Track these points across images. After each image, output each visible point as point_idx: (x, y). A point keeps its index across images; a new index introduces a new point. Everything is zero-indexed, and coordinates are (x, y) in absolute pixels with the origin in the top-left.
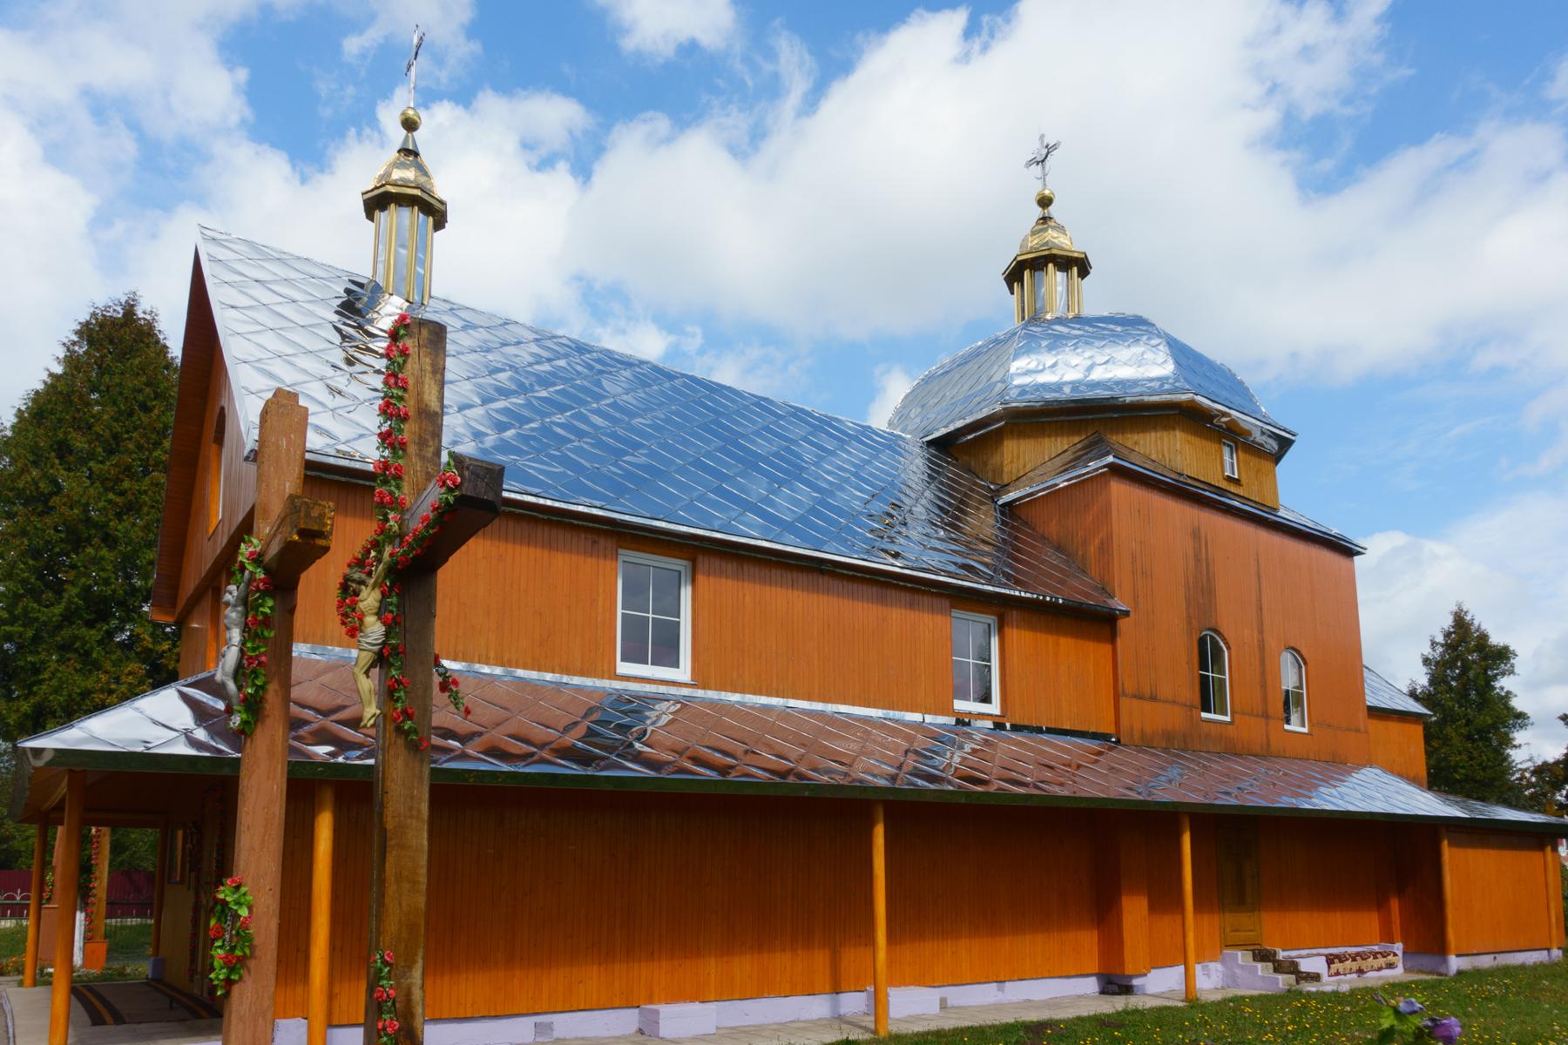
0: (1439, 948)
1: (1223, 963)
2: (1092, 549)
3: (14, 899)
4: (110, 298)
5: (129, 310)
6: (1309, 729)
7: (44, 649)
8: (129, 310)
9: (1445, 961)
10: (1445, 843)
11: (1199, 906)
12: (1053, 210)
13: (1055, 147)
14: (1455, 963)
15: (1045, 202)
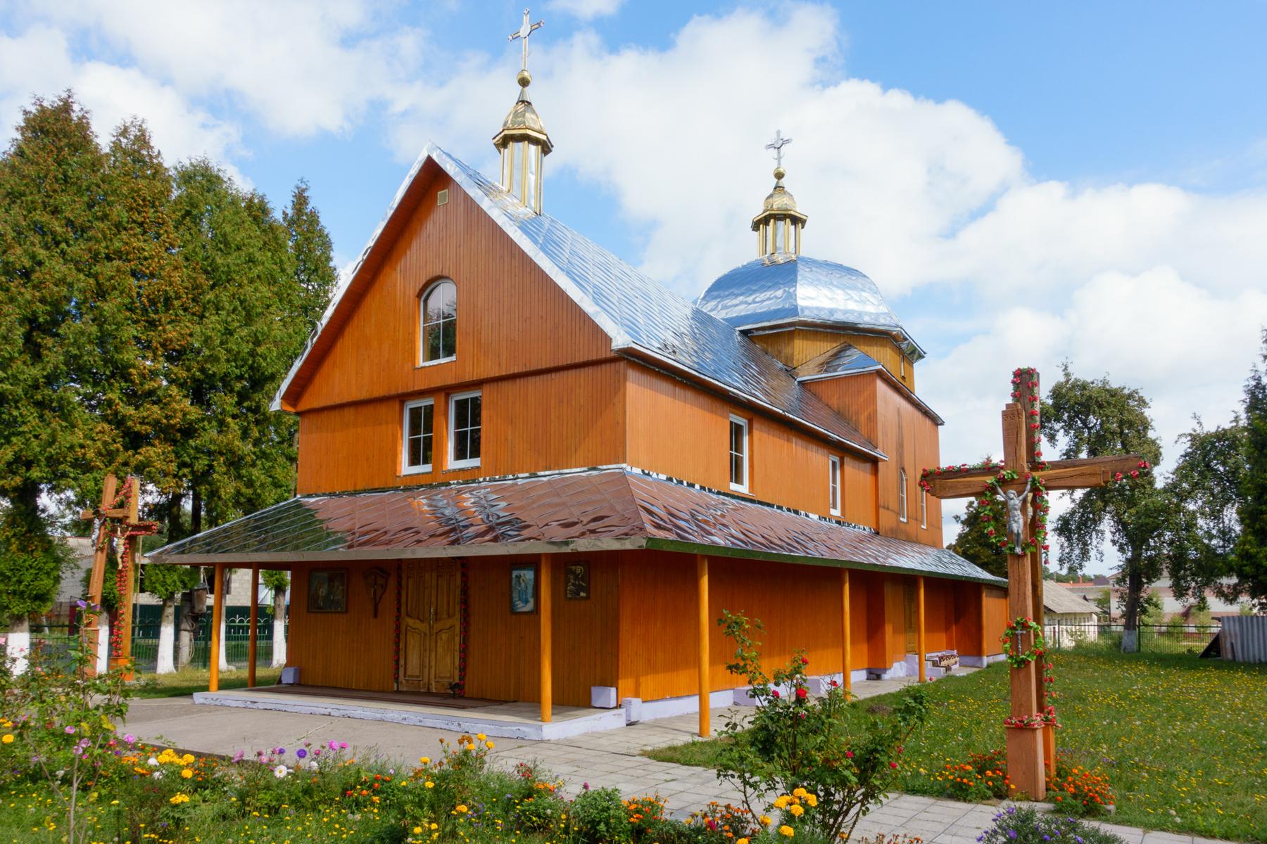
0: (979, 653)
1: (906, 662)
2: (863, 418)
3: (235, 622)
4: (143, 121)
5: (66, 107)
6: (927, 527)
7: (23, 405)
8: (66, 107)
9: (981, 660)
10: (984, 595)
11: (928, 630)
12: (783, 182)
13: (788, 141)
14: (986, 660)
15: (779, 176)
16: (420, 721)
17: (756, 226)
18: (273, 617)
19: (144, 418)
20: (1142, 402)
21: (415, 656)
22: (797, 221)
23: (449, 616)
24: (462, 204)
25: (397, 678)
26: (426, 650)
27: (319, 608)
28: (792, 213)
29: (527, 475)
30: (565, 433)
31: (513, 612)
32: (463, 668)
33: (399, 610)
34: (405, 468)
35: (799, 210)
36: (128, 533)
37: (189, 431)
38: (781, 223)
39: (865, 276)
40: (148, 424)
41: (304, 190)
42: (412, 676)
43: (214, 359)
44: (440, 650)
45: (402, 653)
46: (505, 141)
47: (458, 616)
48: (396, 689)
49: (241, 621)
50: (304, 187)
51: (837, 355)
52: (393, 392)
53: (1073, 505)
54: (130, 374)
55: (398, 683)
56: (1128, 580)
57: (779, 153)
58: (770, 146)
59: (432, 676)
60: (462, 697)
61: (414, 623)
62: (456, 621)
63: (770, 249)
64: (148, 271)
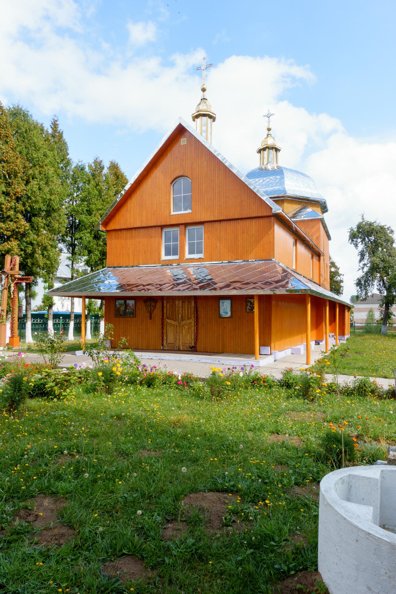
13: (273, 114)
15: (269, 130)
16: (199, 360)
17: (260, 151)
18: (47, 319)
19: (7, 228)
20: (392, 232)
21: (171, 335)
22: (277, 150)
23: (189, 319)
24: (194, 145)
25: (162, 345)
26: (177, 333)
27: (121, 315)
28: (276, 147)
29: (227, 262)
30: (245, 245)
31: (220, 317)
32: (196, 339)
33: (163, 316)
34: (164, 257)
35: (278, 146)
36: (16, 281)
37: (24, 235)
38: (271, 151)
39: (309, 177)
40: (9, 231)
41: (56, 121)
42: (170, 343)
43: (36, 202)
44: (184, 332)
45: (165, 334)
46: (197, 117)
47: (193, 318)
48: (162, 348)
49: (40, 321)
50: (56, 119)
51: (300, 211)
52: (159, 224)
53: (363, 274)
54: (2, 208)
55: (163, 346)
56: (384, 305)
57: (269, 119)
58: (265, 116)
59: (181, 343)
60: (197, 351)
61: (171, 322)
62: (192, 321)
63: (265, 162)
64: (5, 159)
